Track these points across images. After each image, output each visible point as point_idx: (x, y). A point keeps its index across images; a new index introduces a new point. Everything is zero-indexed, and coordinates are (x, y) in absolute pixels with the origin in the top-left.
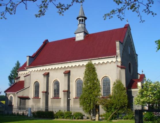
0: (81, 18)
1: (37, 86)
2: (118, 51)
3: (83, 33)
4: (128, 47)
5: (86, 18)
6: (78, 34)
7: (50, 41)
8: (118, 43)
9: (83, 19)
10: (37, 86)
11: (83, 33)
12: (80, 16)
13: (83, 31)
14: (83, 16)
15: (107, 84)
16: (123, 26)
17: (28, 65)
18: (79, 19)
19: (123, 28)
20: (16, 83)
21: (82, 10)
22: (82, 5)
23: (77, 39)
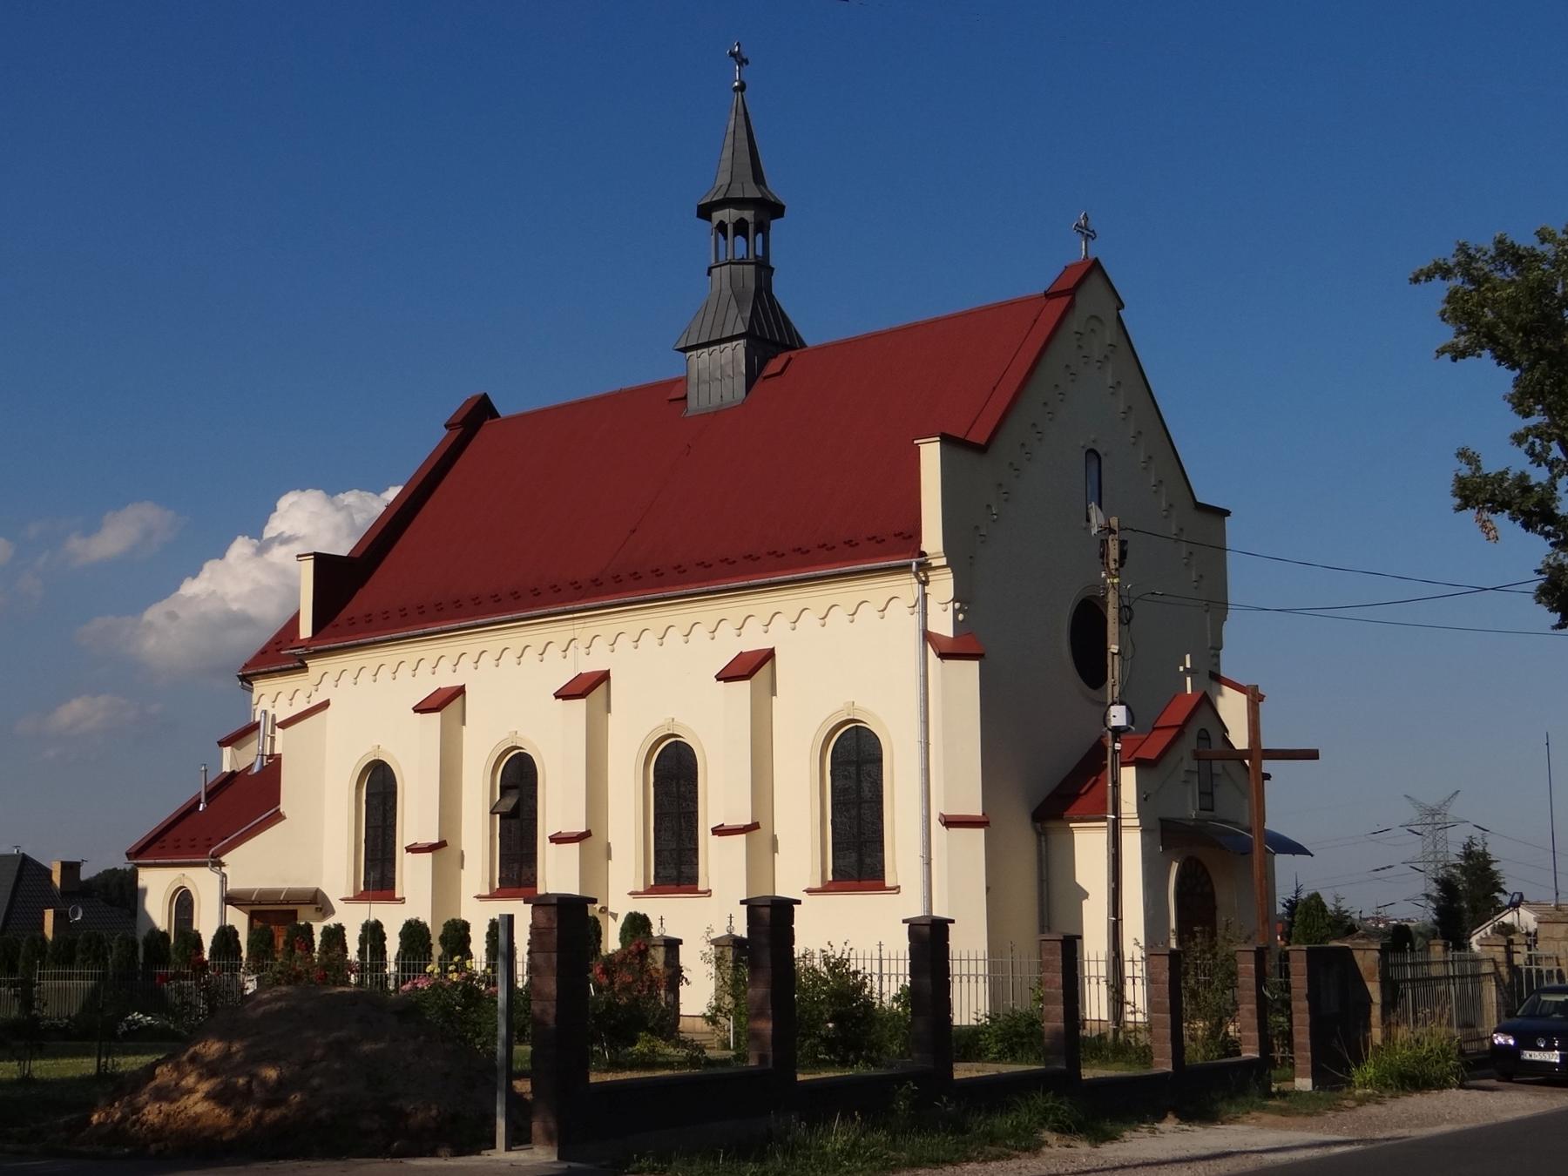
0: (728, 215)
1: (379, 786)
2: (932, 538)
3: (741, 344)
4: (1038, 1060)
5: (777, 210)
6: (705, 352)
7: (506, 407)
8: (930, 454)
9: (748, 215)
10: (379, 786)
11: (742, 342)
12: (719, 197)
13: (741, 329)
14: (752, 192)
15: (859, 782)
16: (1038, 281)
17: (306, 630)
18: (717, 216)
19: (1035, 299)
20: (233, 774)
21: (743, 134)
22: (742, 88)
23: (701, 400)
